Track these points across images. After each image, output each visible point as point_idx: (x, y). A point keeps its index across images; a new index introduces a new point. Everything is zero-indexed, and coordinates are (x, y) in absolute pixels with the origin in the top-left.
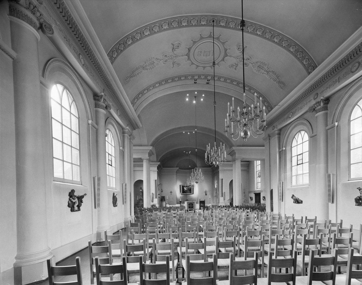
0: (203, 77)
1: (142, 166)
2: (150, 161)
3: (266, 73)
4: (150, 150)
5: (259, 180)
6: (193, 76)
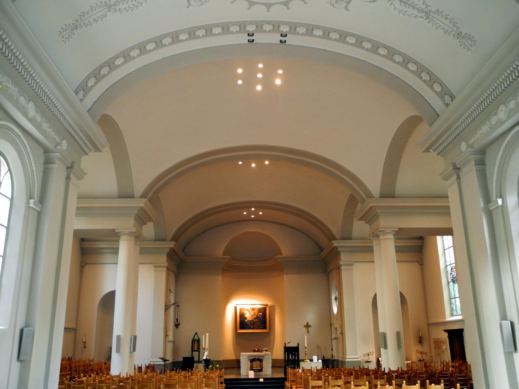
0: (268, 27)
1: (116, 251)
2: (138, 237)
3: (422, 14)
4: (141, 208)
5: (455, 289)
6: (242, 26)
